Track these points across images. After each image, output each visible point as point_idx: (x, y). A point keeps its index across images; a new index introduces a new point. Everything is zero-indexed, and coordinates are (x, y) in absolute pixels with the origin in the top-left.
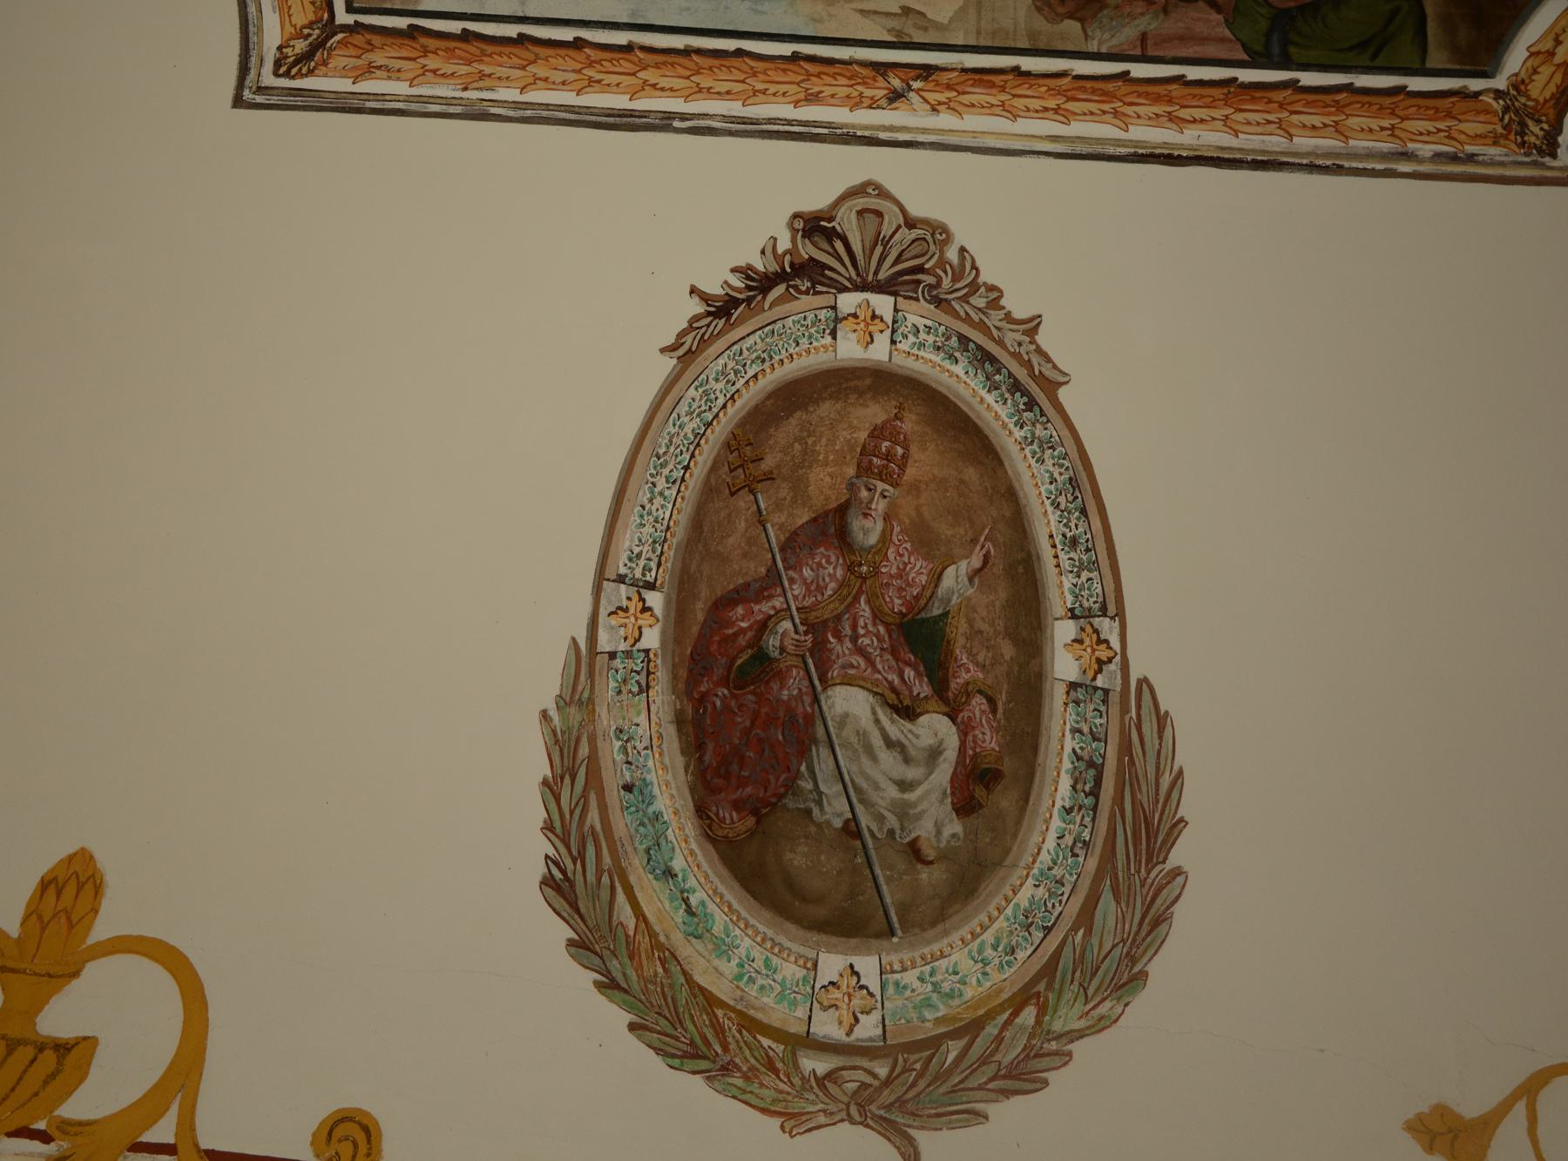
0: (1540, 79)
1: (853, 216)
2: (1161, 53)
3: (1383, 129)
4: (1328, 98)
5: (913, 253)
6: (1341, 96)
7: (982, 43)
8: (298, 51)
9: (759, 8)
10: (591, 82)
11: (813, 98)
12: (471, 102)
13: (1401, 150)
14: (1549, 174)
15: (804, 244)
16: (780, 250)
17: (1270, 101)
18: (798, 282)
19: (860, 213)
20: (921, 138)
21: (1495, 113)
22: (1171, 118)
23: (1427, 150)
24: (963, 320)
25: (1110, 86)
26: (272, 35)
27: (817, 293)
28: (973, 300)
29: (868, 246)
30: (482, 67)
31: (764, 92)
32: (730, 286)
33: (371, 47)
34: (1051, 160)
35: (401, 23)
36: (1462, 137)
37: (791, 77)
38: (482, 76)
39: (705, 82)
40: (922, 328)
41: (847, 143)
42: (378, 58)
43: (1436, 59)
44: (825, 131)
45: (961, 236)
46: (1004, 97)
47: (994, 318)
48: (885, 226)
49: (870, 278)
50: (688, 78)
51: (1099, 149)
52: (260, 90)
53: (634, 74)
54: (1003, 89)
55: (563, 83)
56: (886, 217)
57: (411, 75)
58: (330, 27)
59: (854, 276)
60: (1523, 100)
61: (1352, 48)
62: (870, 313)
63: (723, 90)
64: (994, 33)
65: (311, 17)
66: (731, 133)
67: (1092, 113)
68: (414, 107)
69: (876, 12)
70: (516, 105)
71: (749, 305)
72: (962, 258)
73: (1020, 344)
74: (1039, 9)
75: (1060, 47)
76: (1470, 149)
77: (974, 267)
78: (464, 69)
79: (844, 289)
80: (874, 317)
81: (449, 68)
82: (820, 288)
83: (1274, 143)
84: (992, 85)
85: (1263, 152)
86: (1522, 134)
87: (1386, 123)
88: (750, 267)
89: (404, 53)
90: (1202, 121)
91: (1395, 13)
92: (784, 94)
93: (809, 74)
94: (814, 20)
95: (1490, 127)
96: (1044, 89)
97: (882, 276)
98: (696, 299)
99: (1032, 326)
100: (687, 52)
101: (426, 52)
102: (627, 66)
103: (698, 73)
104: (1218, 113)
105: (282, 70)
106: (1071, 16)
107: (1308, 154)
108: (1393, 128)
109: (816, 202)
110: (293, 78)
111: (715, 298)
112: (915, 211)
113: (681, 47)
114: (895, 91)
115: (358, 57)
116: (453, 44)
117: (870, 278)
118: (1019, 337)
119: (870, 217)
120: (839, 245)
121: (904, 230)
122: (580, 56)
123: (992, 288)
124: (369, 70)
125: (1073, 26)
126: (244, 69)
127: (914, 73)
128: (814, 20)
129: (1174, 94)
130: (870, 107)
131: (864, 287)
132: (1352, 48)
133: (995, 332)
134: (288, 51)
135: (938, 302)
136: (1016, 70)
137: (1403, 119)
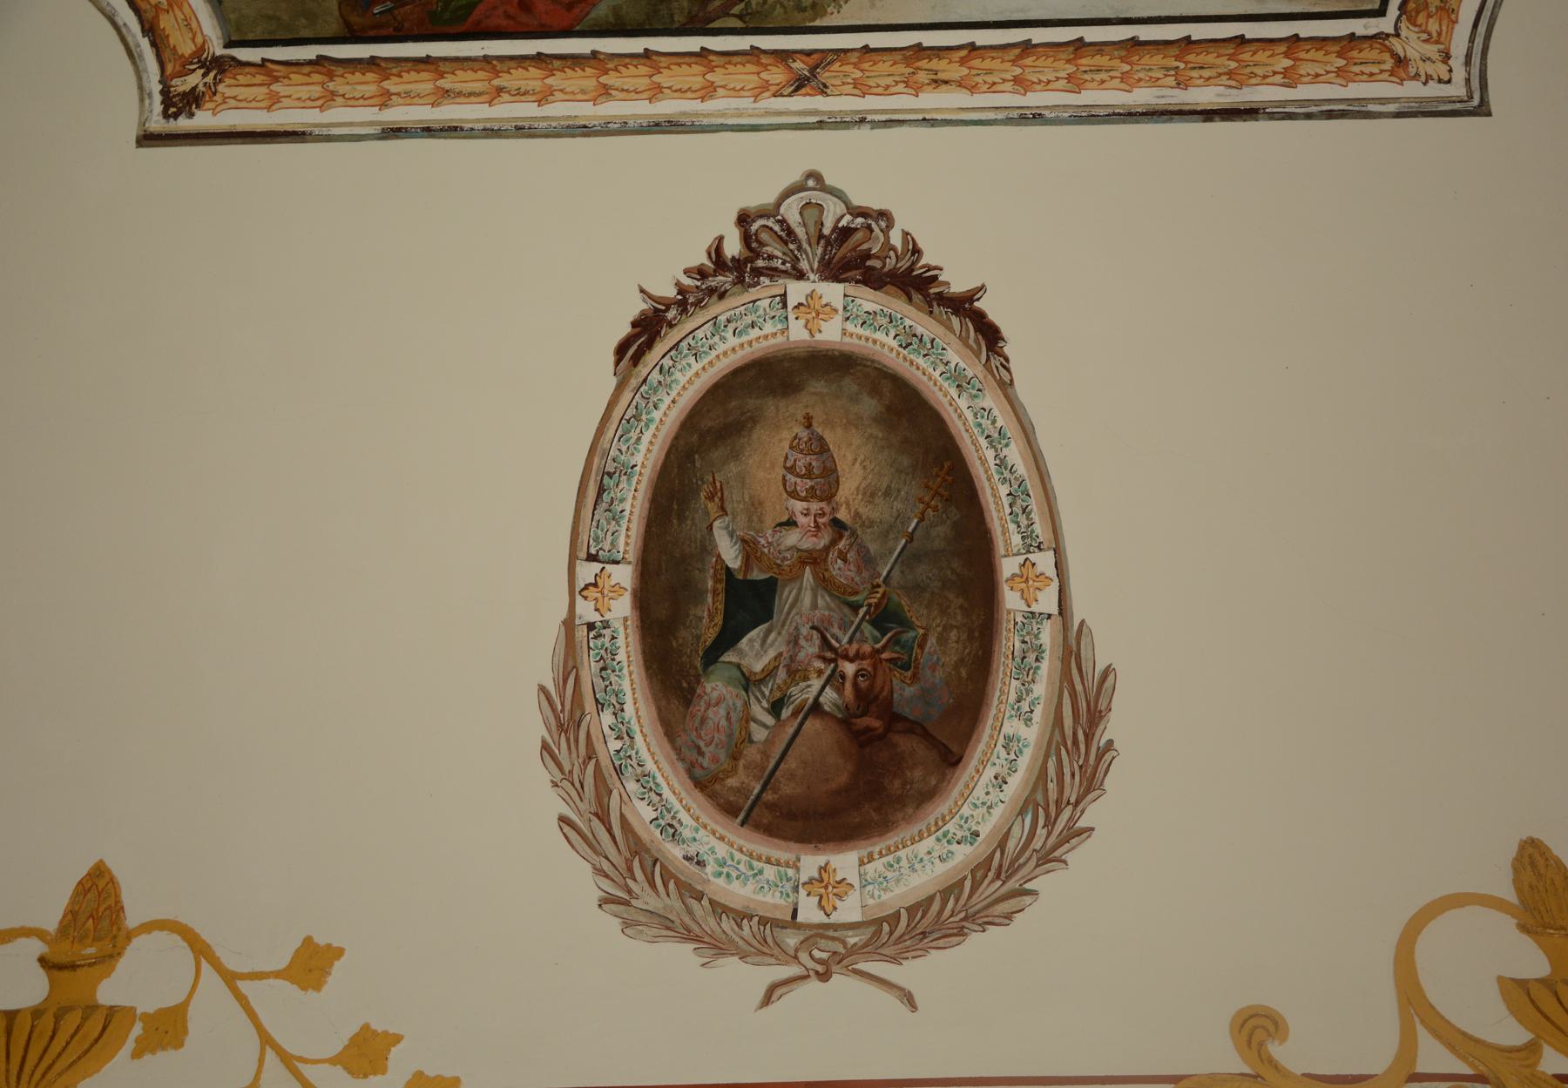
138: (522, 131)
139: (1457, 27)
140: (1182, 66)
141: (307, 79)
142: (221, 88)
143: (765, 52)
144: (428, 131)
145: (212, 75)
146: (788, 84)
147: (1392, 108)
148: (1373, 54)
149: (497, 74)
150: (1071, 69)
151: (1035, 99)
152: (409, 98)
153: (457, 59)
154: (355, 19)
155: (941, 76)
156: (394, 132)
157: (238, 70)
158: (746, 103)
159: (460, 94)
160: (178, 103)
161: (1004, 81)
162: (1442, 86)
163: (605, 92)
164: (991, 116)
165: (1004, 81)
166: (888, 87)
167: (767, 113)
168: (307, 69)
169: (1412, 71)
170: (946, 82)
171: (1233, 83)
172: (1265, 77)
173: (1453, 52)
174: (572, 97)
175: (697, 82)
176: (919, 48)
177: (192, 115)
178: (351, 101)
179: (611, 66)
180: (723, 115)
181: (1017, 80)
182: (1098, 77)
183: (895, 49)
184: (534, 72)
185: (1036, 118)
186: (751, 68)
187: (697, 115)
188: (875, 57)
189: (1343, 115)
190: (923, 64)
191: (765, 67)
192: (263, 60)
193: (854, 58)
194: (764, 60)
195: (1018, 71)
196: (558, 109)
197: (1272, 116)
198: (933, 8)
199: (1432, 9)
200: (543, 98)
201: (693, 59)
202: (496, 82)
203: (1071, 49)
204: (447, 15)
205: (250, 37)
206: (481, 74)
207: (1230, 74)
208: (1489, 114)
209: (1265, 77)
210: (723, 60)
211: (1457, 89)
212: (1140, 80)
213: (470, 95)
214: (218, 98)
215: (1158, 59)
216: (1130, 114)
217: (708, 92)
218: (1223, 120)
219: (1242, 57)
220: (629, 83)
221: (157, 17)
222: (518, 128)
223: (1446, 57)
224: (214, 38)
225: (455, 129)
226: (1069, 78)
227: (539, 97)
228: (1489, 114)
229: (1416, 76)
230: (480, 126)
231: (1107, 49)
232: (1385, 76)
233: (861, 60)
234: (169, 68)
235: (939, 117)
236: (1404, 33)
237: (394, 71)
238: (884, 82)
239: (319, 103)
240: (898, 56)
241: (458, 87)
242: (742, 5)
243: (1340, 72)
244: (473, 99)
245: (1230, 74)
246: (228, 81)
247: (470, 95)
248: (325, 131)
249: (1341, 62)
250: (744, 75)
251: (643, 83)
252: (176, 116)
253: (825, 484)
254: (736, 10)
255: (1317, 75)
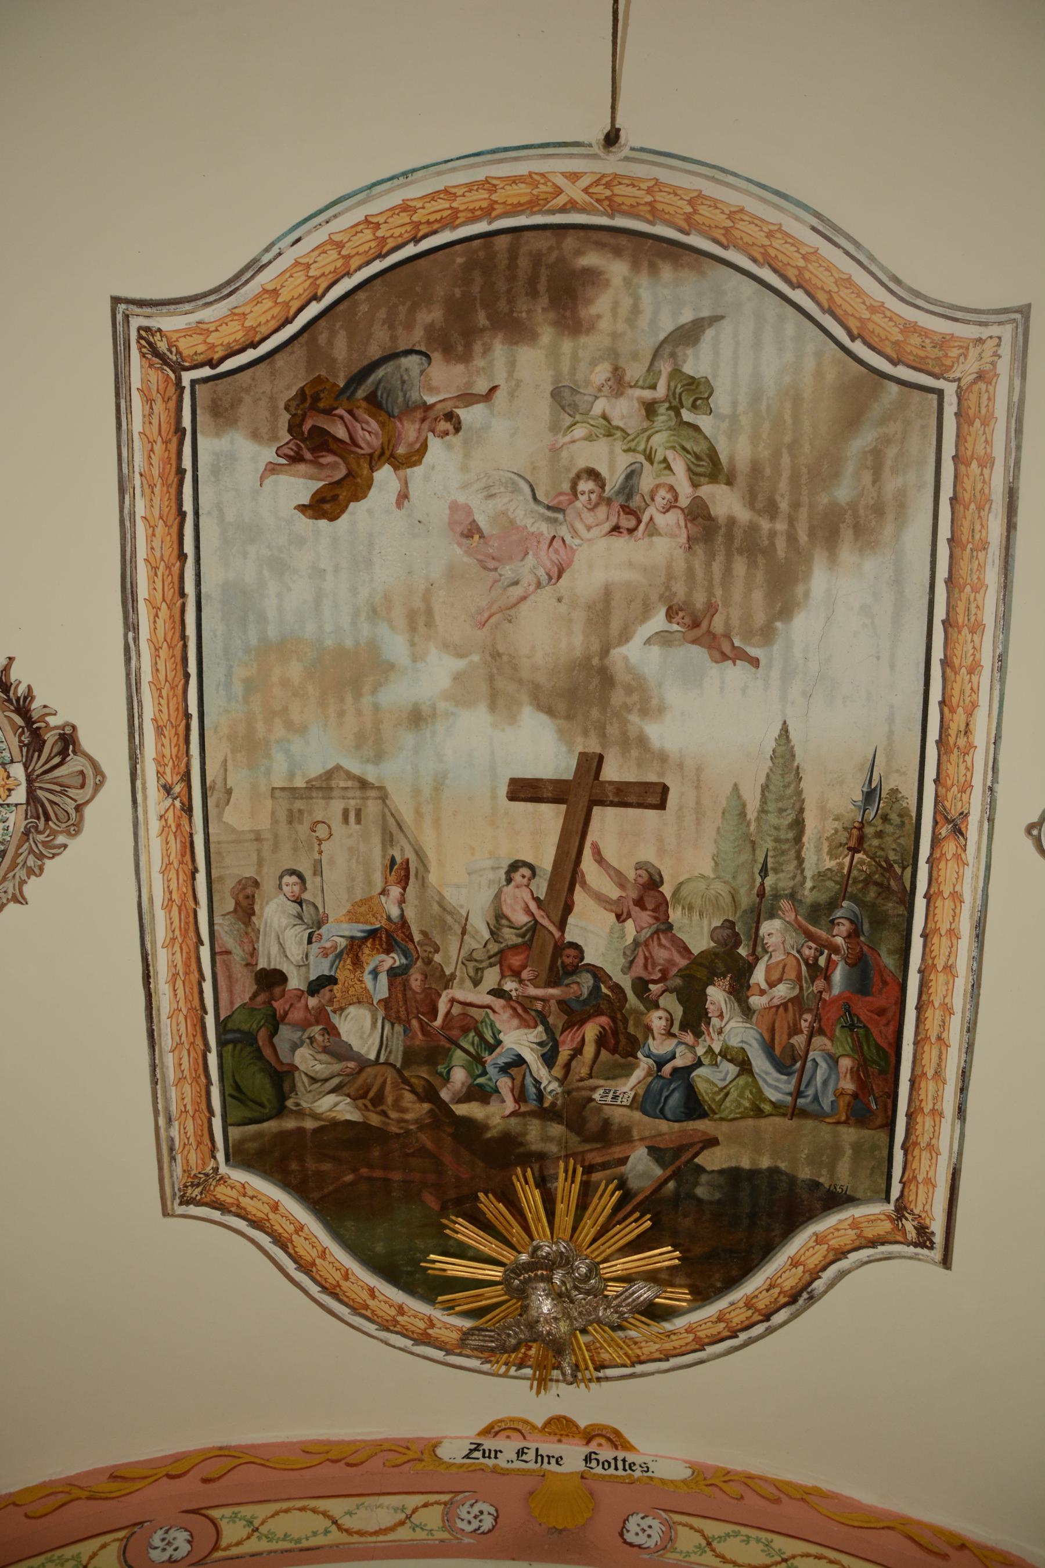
0: (228, 1191)
1: (79, 768)
2: (218, 964)
3: (185, 1106)
4: (201, 1071)
5: (58, 812)
6: (203, 1079)
7: (212, 846)
8: (159, 344)
9: (221, 688)
10: (155, 569)
11: (160, 731)
12: (131, 479)
13: (173, 1118)
14: (169, 1203)
15: (54, 735)
16: (48, 719)
17: (194, 1036)
18: (27, 734)
19: (82, 773)
20: (140, 809)
21: (204, 1169)
22: (175, 975)
23: (175, 1132)
24: (16, 852)
25: (192, 933)
26: (169, 323)
27: (21, 748)
28: (31, 857)
29: (60, 780)
30: (158, 486)
31: (160, 696)
32: (18, 685)
33: (166, 400)
34: (136, 899)
35: (187, 422)
36: (185, 1152)
37: (173, 714)
38: (152, 487)
39: (164, 653)
40: (6, 824)
41: (130, 758)
42: (159, 406)
43: (235, 1132)
44: (137, 742)
45: (74, 844)
46: (176, 864)
47: (22, 873)
48: (74, 791)
49: (37, 785)
50: (165, 640)
51: (147, 930)
52: (126, 317)
53: (164, 600)
54: (181, 863)
55: (152, 548)
56: (81, 791)
57: (148, 433)
58: (178, 368)
59: (36, 773)
60: (214, 1183)
61: (235, 1082)
62: (11, 787)
63: (159, 667)
64: (219, 853)
65: (185, 353)
66: (128, 675)
67: (172, 923)
68: (124, 436)
69: (226, 770)
70: (133, 514)
71: (6, 701)
72: (59, 846)
73: (5, 892)
74: (240, 882)
75: (215, 899)
76: (179, 1158)
77: (54, 855)
78: (155, 472)
79: (26, 767)
80: (10, 790)
81: (155, 460)
82: (25, 750)
83: (167, 1041)
84: (183, 855)
85: (160, 1036)
86: (192, 1185)
87: (189, 1107)
88: (33, 698)
89: (164, 426)
90: (176, 995)
91: (261, 1105)
92: (160, 711)
93: (176, 727)
94: (216, 727)
95: (194, 1167)
96: (184, 890)
97: (39, 793)
98: (5, 662)
99: (19, 899)
100: (184, 637)
101: (166, 442)
102: (169, 594)
103: (169, 647)
104: (182, 1004)
105: (143, 333)
106: (237, 903)
107: (162, 1063)
108: (187, 1112)
109: (86, 740)
110: (138, 342)
111: (8, 676)
112: (88, 811)
113: (187, 633)
114: (171, 788)
115: (158, 392)
116: (174, 462)
117: (37, 785)
118: (10, 891)
119: (80, 780)
120: (57, 760)
121: (74, 804)
122: (174, 558)
123: (41, 869)
124: (149, 401)
125: (230, 905)
126: (141, 303)
127: (186, 801)
128: (216, 727)
129: (192, 975)
130: (158, 772)
131: (30, 781)
132: (235, 1082)
133: (11, 874)
134: (158, 336)
135: (26, 833)
136: (195, 870)
137: (193, 1117)
138: (971, 1028)
139: (957, 334)
140: (970, 546)
141: (917, 1158)
142: (916, 1212)
143: (931, 854)
144: (963, 1090)
145: (907, 1215)
146: (957, 840)
147: (1017, 383)
148: (973, 397)
149: (927, 1038)
150: (965, 630)
151: (987, 659)
152: (937, 1097)
153: (914, 1062)
154: (879, 1121)
155: (962, 728)
156: (961, 1112)
157: (906, 1199)
158: (968, 872)
159: (939, 1065)
160: (924, 1238)
161: (970, 681)
162: (1002, 343)
163: (949, 968)
164: (996, 693)
165: (970, 681)
166: (967, 768)
167: (978, 857)
168: (910, 1158)
169: (989, 367)
170: (968, 724)
171: (987, 507)
172: (984, 482)
173: (976, 336)
174: (950, 992)
175: (948, 904)
176: (940, 743)
177: (933, 1233)
178: (936, 1133)
179: (930, 962)
180: (976, 889)
181: (971, 672)
182: (973, 610)
183: (939, 760)
184: (929, 1013)
185: (1001, 661)
186: (942, 865)
187: (973, 907)
188: (943, 775)
189: (1019, 421)
190: (951, 740)
191: (943, 855)
192: (900, 1182)
193: (942, 791)
194: (937, 855)
195: (964, 670)
196: (958, 1002)
197: (1016, 477)
198: (910, 730)
199: (941, 354)
200: (948, 1010)
201: (932, 905)
202: (933, 1040)
203: (950, 629)
204: (882, 1063)
205: (884, 1186)
206: (927, 1048)
207: (980, 508)
208: (1029, 305)
209: (984, 482)
210: (934, 884)
211: (1006, 332)
212: (978, 578)
213: (940, 1058)
214: (923, 1215)
215: (963, 565)
216: (1005, 587)
217: (957, 897)
218: (1016, 515)
219: (967, 499)
220: (944, 951)
221: (865, 1238)
222: (968, 1031)
223: (980, 341)
224: (882, 1208)
225: (963, 1072)
226: (972, 632)
227: (947, 1014)
228: (1029, 305)
229: (993, 364)
230: (964, 1056)
231: (952, 603)
232: (991, 388)
233: (944, 786)
234: (900, 1239)
235: (994, 732)
236: (958, 375)
237: (917, 1103)
238: (962, 770)
239: (934, 1155)
240: (944, 758)
241: (934, 1065)
242: (895, 866)
243: (985, 423)
244: (944, 1057)
245: (980, 508)
246: (912, 1206)
247: (940, 1058)
248: (955, 1155)
249: (977, 423)
250: (947, 871)
251: (945, 942)
252: (932, 1243)
253: (810, 948)
254: (899, 871)
255: (986, 441)
